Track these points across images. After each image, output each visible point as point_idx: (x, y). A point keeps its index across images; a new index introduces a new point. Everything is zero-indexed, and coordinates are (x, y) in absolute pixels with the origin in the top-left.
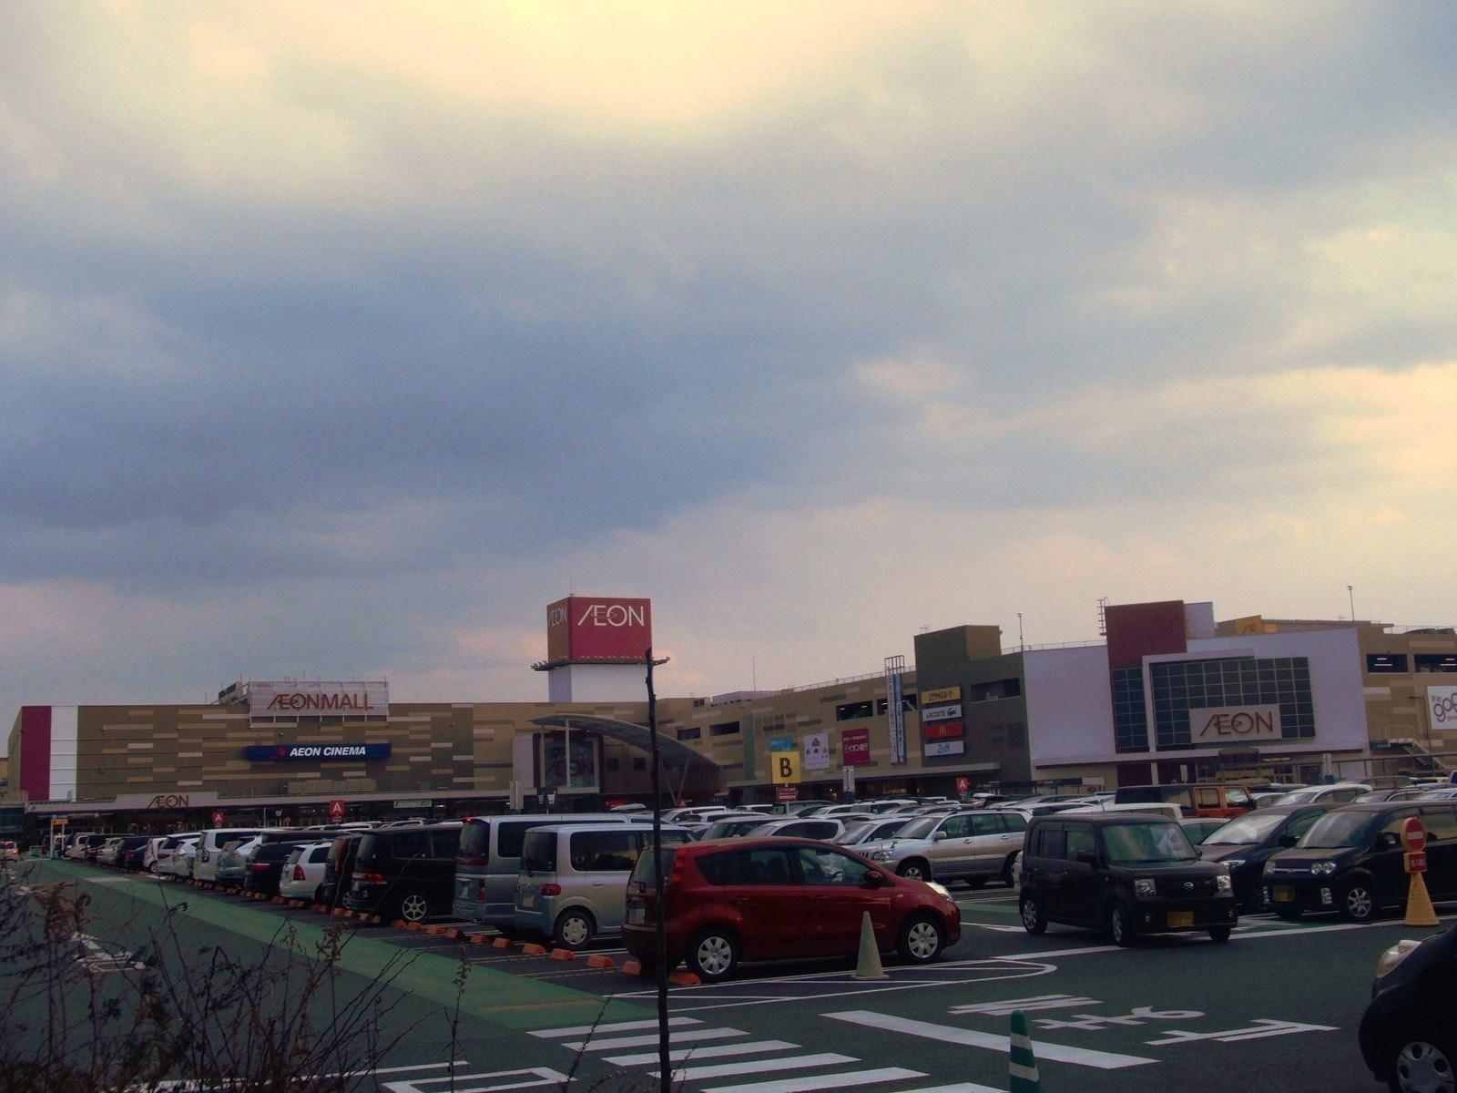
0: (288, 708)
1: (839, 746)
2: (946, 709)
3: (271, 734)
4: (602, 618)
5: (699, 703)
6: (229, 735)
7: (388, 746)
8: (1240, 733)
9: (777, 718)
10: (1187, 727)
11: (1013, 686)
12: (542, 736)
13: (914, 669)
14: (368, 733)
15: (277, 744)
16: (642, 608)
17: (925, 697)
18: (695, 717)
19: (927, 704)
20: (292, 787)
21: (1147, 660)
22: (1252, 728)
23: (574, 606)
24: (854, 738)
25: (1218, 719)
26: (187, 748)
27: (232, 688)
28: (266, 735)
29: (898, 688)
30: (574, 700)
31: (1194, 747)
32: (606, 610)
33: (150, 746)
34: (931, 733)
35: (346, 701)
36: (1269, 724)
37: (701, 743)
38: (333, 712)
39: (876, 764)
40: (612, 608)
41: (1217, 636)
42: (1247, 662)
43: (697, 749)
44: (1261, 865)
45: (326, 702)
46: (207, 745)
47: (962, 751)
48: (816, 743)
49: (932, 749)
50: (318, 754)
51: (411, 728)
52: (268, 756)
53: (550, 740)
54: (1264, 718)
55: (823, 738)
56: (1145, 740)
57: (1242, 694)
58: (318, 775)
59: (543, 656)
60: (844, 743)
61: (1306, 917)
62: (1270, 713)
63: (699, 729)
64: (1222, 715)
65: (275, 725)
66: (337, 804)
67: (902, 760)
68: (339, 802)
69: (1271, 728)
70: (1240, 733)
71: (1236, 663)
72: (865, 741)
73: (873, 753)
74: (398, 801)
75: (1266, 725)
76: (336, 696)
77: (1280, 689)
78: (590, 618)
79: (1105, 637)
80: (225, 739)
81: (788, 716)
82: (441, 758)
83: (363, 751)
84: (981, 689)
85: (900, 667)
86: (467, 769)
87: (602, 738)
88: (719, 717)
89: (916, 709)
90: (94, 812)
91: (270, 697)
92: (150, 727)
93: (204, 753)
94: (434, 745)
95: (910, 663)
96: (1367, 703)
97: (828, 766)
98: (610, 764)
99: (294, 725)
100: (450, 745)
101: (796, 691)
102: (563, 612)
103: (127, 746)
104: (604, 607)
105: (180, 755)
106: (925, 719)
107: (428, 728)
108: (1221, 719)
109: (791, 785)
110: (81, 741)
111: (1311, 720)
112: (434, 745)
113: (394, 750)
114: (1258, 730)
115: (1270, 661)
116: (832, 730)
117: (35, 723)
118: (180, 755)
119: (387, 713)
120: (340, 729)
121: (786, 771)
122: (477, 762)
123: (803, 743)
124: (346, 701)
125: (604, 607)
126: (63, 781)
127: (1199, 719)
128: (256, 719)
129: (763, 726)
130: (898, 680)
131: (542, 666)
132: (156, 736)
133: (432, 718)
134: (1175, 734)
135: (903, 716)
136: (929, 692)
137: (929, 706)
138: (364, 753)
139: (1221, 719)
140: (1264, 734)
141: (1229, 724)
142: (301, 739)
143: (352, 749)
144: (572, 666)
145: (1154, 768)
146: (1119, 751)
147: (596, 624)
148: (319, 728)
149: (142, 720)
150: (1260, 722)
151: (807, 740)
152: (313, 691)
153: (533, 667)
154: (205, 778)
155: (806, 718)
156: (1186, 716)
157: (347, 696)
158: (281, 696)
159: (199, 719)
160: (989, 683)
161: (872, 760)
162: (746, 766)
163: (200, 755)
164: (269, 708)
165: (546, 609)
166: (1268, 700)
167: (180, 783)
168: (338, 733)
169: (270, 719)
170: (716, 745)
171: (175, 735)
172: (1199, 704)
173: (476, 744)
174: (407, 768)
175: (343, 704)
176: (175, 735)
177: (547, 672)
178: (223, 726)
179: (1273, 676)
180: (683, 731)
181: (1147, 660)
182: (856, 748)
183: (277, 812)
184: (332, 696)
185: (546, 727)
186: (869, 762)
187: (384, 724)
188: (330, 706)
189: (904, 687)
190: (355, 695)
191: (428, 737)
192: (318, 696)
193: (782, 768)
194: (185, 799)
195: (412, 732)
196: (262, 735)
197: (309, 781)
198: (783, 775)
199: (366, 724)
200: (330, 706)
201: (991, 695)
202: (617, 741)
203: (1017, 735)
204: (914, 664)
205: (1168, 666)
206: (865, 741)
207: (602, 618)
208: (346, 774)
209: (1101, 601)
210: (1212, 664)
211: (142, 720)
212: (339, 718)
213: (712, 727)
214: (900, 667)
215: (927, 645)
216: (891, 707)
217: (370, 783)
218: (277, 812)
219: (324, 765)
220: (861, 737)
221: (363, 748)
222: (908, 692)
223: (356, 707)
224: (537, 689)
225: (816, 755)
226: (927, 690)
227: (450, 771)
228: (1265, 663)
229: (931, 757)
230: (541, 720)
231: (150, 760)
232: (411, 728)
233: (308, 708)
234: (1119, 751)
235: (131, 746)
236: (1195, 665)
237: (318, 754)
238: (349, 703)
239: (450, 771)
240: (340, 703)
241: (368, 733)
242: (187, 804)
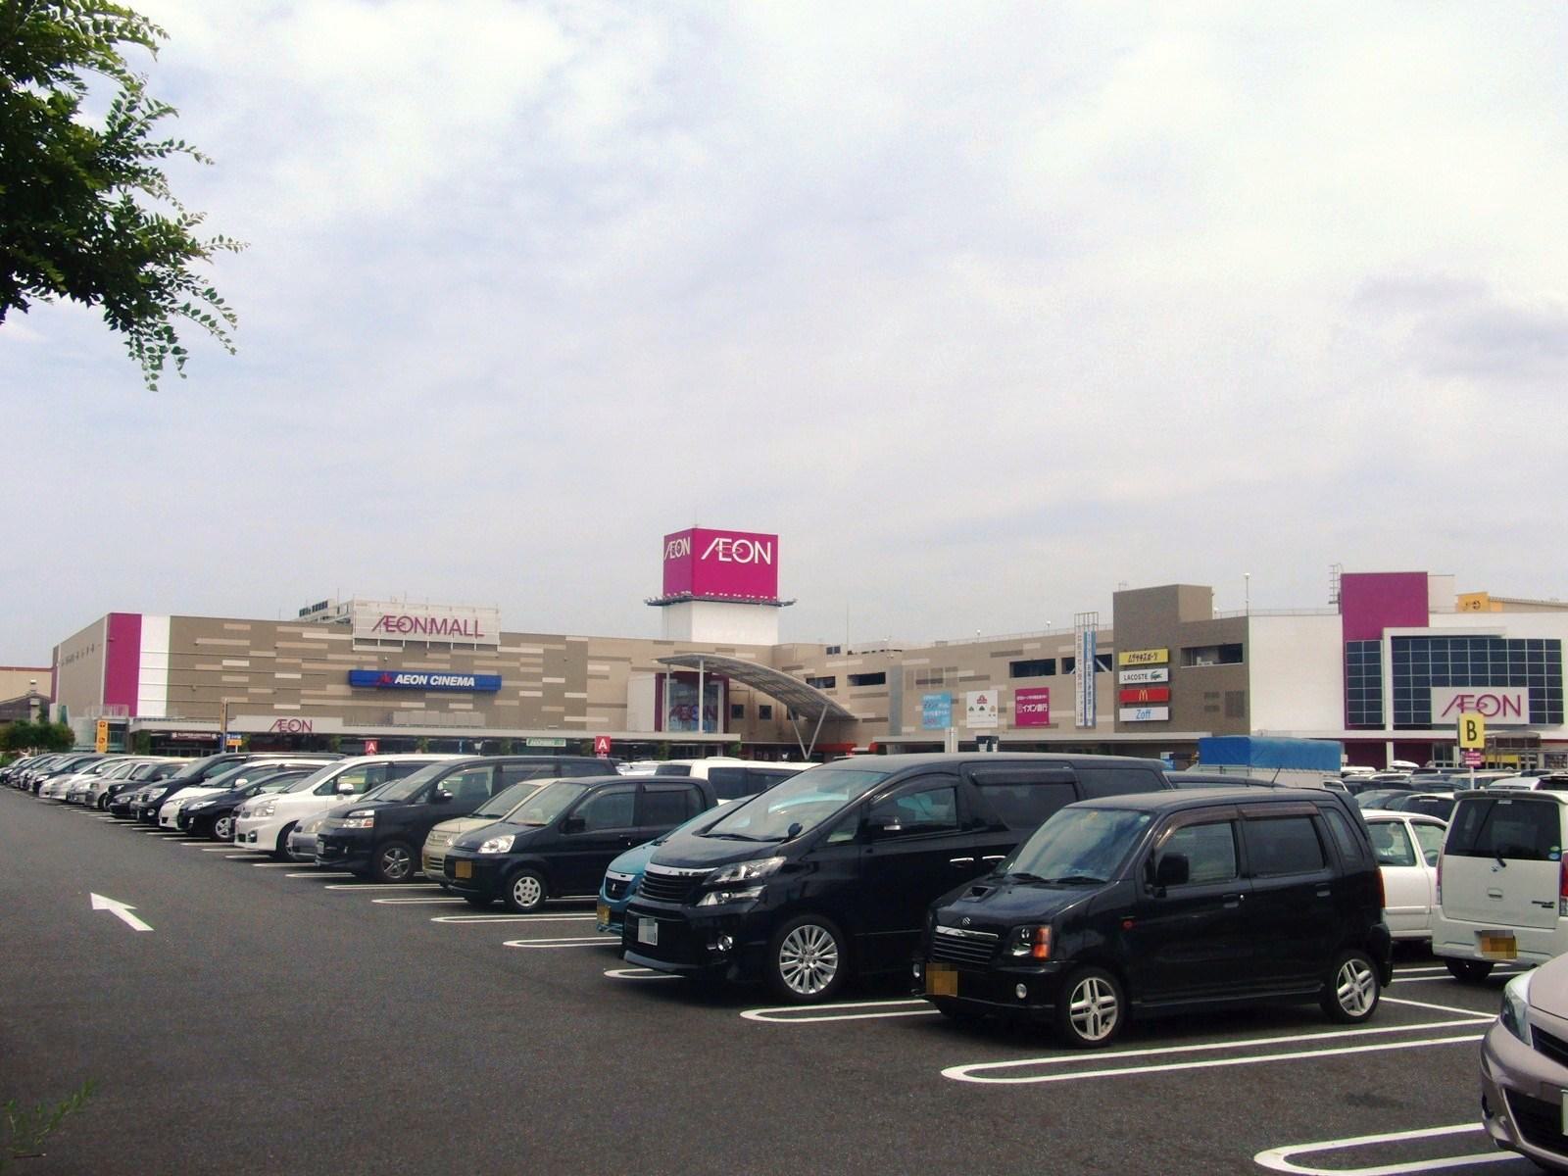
0: (394, 631)
1: (1011, 704)
2: (1149, 672)
3: (375, 658)
4: (727, 553)
5: (834, 651)
6: (330, 657)
7: (498, 679)
8: (1486, 715)
9: (933, 670)
10: (1427, 706)
11: (1234, 653)
12: (668, 676)
13: (1112, 628)
14: (476, 663)
15: (381, 670)
16: (704, 557)
17: (1124, 658)
18: (828, 665)
19: (1126, 666)
20: (397, 717)
21: (1389, 632)
22: (1498, 710)
23: (700, 538)
24: (1030, 697)
25: (1462, 700)
26: (285, 668)
27: (324, 605)
28: (369, 660)
29: (1089, 646)
30: (695, 639)
31: (1430, 727)
32: (731, 544)
33: (246, 663)
34: (1128, 696)
35: (456, 627)
36: (1516, 706)
37: (836, 693)
38: (442, 638)
39: (1056, 726)
40: (738, 542)
41: (1457, 612)
42: (1497, 642)
43: (831, 698)
44: (480, 845)
45: (434, 627)
46: (306, 666)
47: (1167, 718)
48: (982, 700)
49: (1129, 714)
50: (425, 683)
51: (523, 660)
52: (372, 683)
53: (675, 681)
54: (1513, 703)
55: (992, 697)
56: (1379, 717)
57: (1431, 675)
58: (422, 705)
59: (658, 592)
60: (1018, 702)
61: (497, 904)
62: (1519, 697)
63: (834, 678)
64: (1467, 696)
65: (380, 648)
66: (603, 741)
67: (1090, 724)
68: (606, 739)
69: (1518, 712)
70: (1486, 715)
71: (1408, 642)
72: (1046, 701)
73: (1052, 715)
74: (531, 738)
75: (1516, 711)
76: (445, 621)
77: (1360, 668)
78: (714, 553)
79: (1337, 605)
80: (325, 661)
81: (948, 670)
82: (553, 694)
83: (471, 682)
84: (1191, 653)
85: (1094, 624)
86: (580, 707)
87: (728, 682)
88: (860, 666)
89: (1111, 670)
90: (212, 733)
91: (374, 618)
92: (247, 643)
93: (303, 675)
94: (545, 680)
95: (1106, 620)
96: (1016, 676)
97: (996, 726)
98: (735, 712)
99: (399, 650)
100: (562, 680)
101: (949, 644)
102: (686, 545)
103: (221, 663)
104: (730, 540)
105: (278, 675)
106: (1122, 681)
107: (541, 661)
108: (1466, 700)
109: (1476, 750)
110: (172, 655)
111: (1560, 706)
112: (545, 680)
113: (504, 683)
114: (1505, 714)
115: (1522, 641)
116: (1004, 688)
117: (124, 631)
118: (278, 675)
119: (499, 643)
120: (447, 657)
121: (1472, 735)
122: (588, 701)
123: (965, 700)
124: (455, 627)
125: (730, 540)
126: (152, 703)
127: (1441, 698)
128: (359, 641)
129: (915, 678)
130: (1089, 639)
131: (657, 601)
132: (252, 653)
133: (545, 650)
134: (1411, 711)
135: (1094, 676)
136: (1129, 654)
137: (1126, 668)
138: (473, 684)
139: (1466, 700)
140: (1511, 719)
141: (1474, 705)
142: (406, 665)
143: (461, 679)
144: (693, 602)
145: (1390, 747)
146: (1347, 727)
147: (721, 558)
148: (426, 654)
149: (239, 635)
150: (1508, 705)
151: (971, 697)
152: (421, 614)
153: (646, 601)
154: (303, 701)
155: (971, 673)
156: (1427, 694)
157: (456, 621)
158: (388, 617)
159: (299, 638)
160: (1200, 648)
161: (1051, 721)
162: (894, 722)
163: (299, 676)
164: (374, 630)
165: (663, 540)
166: (1517, 682)
167: (277, 706)
168: (446, 662)
169: (374, 642)
170: (853, 696)
171: (272, 654)
172: (1442, 682)
173: (590, 682)
174: (516, 703)
175: (452, 629)
176: (272, 654)
177: (660, 608)
178: (325, 646)
179: (1543, 657)
180: (814, 679)
181: (1389, 632)
182: (1033, 708)
183: (476, 745)
184: (441, 620)
185: (672, 666)
186: (1048, 724)
187: (493, 654)
188: (438, 632)
189: (1100, 646)
190: (466, 621)
191: (540, 670)
192: (426, 619)
193: (1469, 731)
194: (308, 724)
195: (524, 665)
196: (365, 658)
197: (415, 712)
198: (1469, 739)
199: (476, 652)
200: (438, 632)
201: (1202, 661)
202: (745, 686)
203: (1238, 704)
204: (1112, 622)
205: (1449, 639)
206: (1046, 701)
207: (727, 553)
208: (452, 706)
209: (1333, 566)
210: (1459, 641)
211: (239, 635)
212: (447, 645)
213: (850, 677)
214: (1094, 624)
215: (1127, 603)
216: (1079, 666)
217: (479, 717)
218: (476, 745)
219: (429, 695)
220: (1040, 697)
221: (472, 679)
222: (1100, 652)
223: (466, 634)
224: (653, 625)
225: (980, 713)
226: (1126, 651)
227: (562, 709)
228: (1517, 644)
229: (1126, 722)
230: (669, 659)
231: (245, 679)
232: (523, 660)
233: (416, 632)
234: (1347, 727)
235: (226, 663)
236: (1440, 641)
237: (425, 683)
238: (459, 630)
239: (562, 709)
240: (449, 629)
241: (476, 663)
242: (310, 730)
